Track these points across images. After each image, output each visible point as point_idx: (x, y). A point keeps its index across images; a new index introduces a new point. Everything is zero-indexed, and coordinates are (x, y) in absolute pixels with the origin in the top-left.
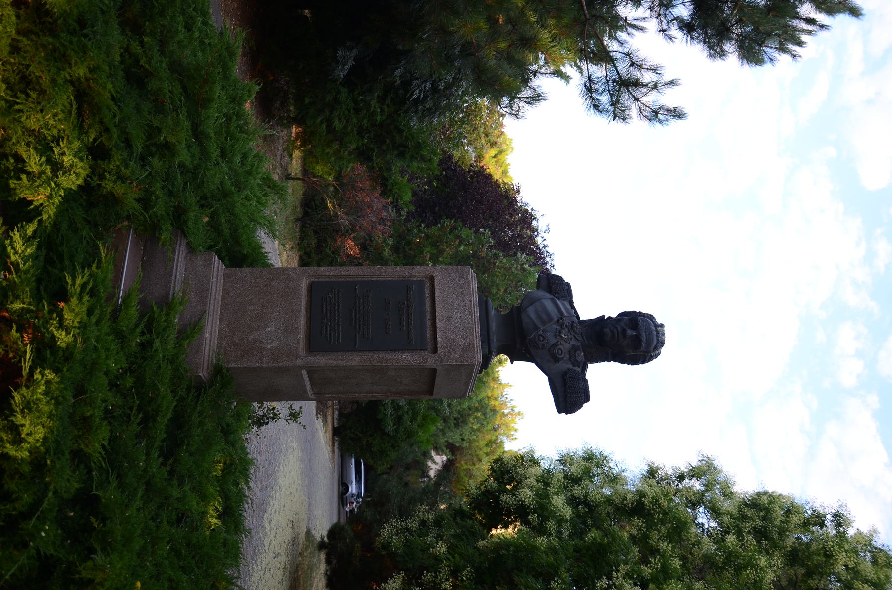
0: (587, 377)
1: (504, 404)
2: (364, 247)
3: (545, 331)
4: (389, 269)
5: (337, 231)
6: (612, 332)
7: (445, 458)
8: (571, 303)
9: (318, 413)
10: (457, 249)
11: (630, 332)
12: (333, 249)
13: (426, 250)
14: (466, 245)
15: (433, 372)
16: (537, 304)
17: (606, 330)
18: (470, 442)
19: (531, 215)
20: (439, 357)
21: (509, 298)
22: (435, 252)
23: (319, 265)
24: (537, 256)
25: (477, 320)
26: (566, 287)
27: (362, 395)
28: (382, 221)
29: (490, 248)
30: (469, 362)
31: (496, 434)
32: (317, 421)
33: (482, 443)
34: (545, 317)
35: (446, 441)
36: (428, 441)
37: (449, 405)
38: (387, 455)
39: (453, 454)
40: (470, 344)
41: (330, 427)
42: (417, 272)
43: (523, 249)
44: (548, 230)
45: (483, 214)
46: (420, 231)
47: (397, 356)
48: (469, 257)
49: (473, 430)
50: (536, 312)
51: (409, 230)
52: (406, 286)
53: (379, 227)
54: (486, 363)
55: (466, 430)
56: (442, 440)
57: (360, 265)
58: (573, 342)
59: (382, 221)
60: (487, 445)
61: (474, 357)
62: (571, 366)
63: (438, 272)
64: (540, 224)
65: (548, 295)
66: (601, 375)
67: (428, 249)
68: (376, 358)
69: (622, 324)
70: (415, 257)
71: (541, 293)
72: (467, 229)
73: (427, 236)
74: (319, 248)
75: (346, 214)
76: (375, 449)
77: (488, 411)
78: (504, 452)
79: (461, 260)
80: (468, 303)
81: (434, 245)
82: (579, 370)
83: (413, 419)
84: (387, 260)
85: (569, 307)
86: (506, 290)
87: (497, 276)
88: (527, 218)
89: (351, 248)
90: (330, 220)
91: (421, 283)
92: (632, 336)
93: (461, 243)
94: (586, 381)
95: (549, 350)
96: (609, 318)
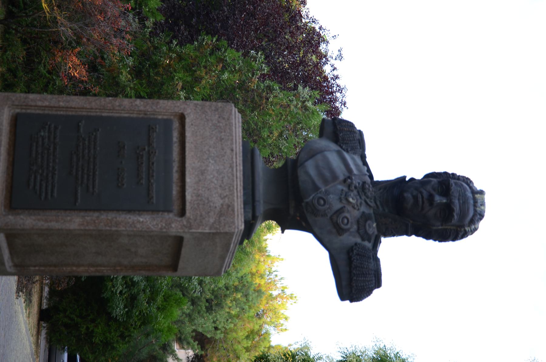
0: (379, 255)
1: (272, 284)
2: (93, 68)
4: (126, 102)
5: (56, 43)
6: (415, 198)
7: (191, 353)
8: (363, 157)
9: (19, 290)
10: (218, 77)
11: (438, 199)
12: (49, 67)
13: (178, 76)
14: (231, 72)
15: (179, 241)
16: (319, 157)
17: (408, 195)
18: (226, 332)
19: (319, 35)
20: (188, 222)
21: (284, 145)
22: (189, 79)
23: (29, 91)
24: (325, 90)
25: (240, 174)
26: (357, 136)
27: (81, 269)
28: (118, 33)
29: (263, 77)
30: (227, 229)
31: (261, 322)
32: (17, 301)
33: (242, 334)
34: (327, 174)
35: (194, 331)
36: (170, 329)
37: (200, 283)
38: (113, 348)
39: (203, 348)
40: (229, 206)
41: (35, 309)
42: (164, 108)
43: (307, 80)
44: (340, 57)
45: (256, 30)
46: (170, 50)
47: (131, 218)
48: (234, 89)
49: (231, 316)
50: (317, 167)
51: (156, 48)
52: (149, 126)
53: (114, 41)
54: (248, 232)
55: (221, 315)
56: (188, 329)
57: (85, 93)
58: (363, 209)
59: (118, 33)
60: (247, 337)
61: (233, 223)
62: (359, 240)
63: (192, 110)
64: (330, 48)
65: (333, 146)
66: (397, 253)
67: (180, 75)
68: (104, 220)
69: (429, 188)
70: (162, 84)
71: (325, 143)
72: (234, 51)
73: (180, 58)
74: (30, 63)
75: (70, 19)
76: (96, 340)
77: (251, 291)
78: (270, 347)
79: (224, 94)
80: (229, 152)
81: (189, 69)
83: (151, 300)
84: (125, 86)
85: (360, 163)
86: (281, 135)
88: (313, 39)
89: (74, 66)
90: (46, 26)
91: (167, 123)
92: (441, 204)
93: (224, 69)
94: (377, 261)
95: (331, 218)
96: (412, 179)
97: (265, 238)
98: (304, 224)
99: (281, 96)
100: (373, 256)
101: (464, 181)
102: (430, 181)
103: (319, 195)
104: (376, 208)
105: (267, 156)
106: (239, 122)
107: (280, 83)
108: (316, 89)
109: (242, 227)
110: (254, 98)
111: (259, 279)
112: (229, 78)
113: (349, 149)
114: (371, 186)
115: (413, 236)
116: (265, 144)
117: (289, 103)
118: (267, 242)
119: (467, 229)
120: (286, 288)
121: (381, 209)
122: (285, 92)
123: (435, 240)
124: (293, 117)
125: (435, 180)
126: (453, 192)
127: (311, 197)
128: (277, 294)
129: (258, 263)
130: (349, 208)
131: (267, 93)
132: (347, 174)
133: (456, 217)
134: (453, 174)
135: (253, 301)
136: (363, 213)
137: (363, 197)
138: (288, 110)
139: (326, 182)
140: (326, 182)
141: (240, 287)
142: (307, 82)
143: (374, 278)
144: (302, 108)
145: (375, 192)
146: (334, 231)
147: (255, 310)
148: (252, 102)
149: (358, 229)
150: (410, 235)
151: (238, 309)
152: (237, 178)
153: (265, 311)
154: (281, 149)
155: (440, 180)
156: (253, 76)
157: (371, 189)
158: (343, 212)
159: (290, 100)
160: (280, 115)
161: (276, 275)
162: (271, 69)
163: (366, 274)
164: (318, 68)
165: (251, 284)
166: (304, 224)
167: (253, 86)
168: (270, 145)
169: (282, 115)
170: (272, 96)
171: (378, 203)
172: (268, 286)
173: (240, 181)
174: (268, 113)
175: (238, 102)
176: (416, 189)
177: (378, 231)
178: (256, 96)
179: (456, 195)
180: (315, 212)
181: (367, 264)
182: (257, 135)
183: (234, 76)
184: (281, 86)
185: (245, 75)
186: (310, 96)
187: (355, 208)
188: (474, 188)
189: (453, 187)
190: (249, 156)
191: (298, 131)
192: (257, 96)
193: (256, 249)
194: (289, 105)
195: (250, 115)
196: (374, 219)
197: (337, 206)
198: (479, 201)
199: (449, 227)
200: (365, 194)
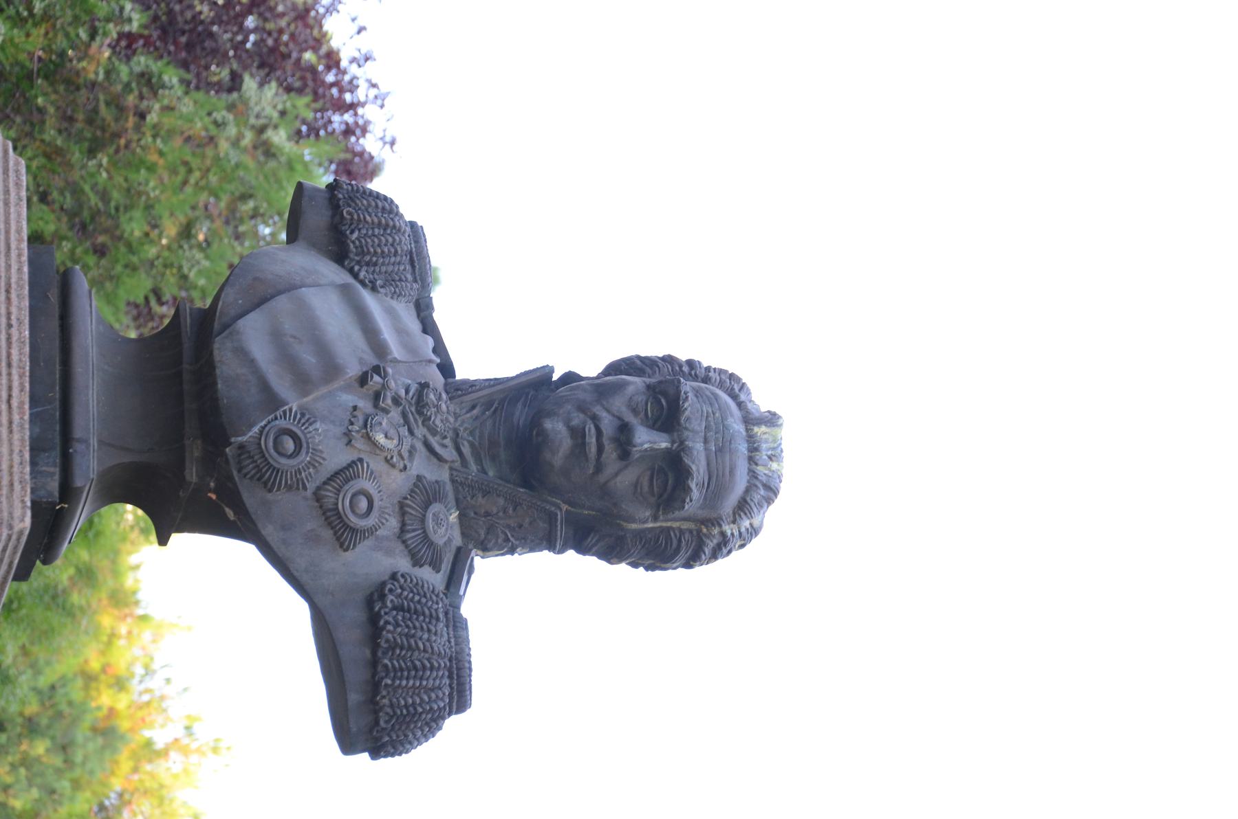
0: (466, 610)
1: (149, 707)
3: (307, 417)
6: (578, 434)
8: (423, 309)
17: (555, 427)
26: (406, 244)
29: (128, 44)
34: (308, 358)
43: (270, 61)
48: (29, 77)
58: (421, 466)
62: (403, 564)
65: (331, 272)
66: (529, 608)
69: (619, 404)
82: (434, 579)
85: (414, 326)
86: (187, 232)
87: (151, 169)
92: (653, 454)
94: (457, 625)
96: (570, 378)
97: (133, 559)
98: (230, 514)
99: (187, 106)
100: (446, 613)
101: (721, 385)
102: (621, 386)
103: (282, 423)
104: (457, 465)
105: (141, 300)
106: (18, 185)
107: (185, 65)
108: (300, 91)
109: (25, 523)
110: (95, 111)
111: (111, 692)
112: (11, 40)
113: (379, 283)
114: (444, 396)
115: (571, 553)
116: (135, 259)
117: (213, 131)
118: (140, 574)
119: (728, 529)
120: (196, 719)
121: (474, 467)
122: (200, 95)
123: (635, 565)
124: (226, 178)
125: (636, 383)
126: (688, 419)
127: (256, 429)
128: (170, 739)
129: (109, 643)
130: (376, 464)
131: (141, 97)
132: (372, 360)
133: (695, 494)
134: (690, 363)
135: (89, 766)
136: (419, 478)
137: (420, 431)
138: (210, 152)
139: (303, 382)
140: (303, 382)
141: (44, 721)
142: (272, 69)
143: (446, 681)
144: (255, 147)
145: (456, 416)
146: (327, 534)
147: (94, 793)
148: (90, 121)
149: (403, 529)
150: (561, 551)
151: (35, 793)
152: (9, 365)
153: (127, 797)
154: (184, 277)
155: (653, 380)
156: (92, 36)
157: (444, 407)
158: (357, 476)
159: (215, 123)
160: (182, 170)
161: (168, 681)
162: (156, 18)
163: (424, 667)
164: (307, 26)
165: (80, 710)
166: (230, 514)
167: (93, 70)
168: (152, 264)
169: (190, 171)
170: (157, 106)
171: (466, 450)
172: (140, 714)
173: (21, 376)
174: (142, 162)
175: (43, 122)
176: (582, 408)
177: (464, 534)
178: (102, 107)
179: (697, 425)
180: (267, 477)
181: (426, 636)
182: (106, 231)
183: (28, 35)
184: (188, 77)
185: (67, 35)
186: (283, 113)
187: (393, 467)
188: (750, 406)
189: (691, 407)
190: (54, 297)
191: (241, 221)
192: (108, 104)
193: (104, 595)
194: (211, 139)
195: (84, 167)
196: (451, 496)
197: (336, 457)
198: (764, 446)
199: (676, 525)
200: (426, 420)
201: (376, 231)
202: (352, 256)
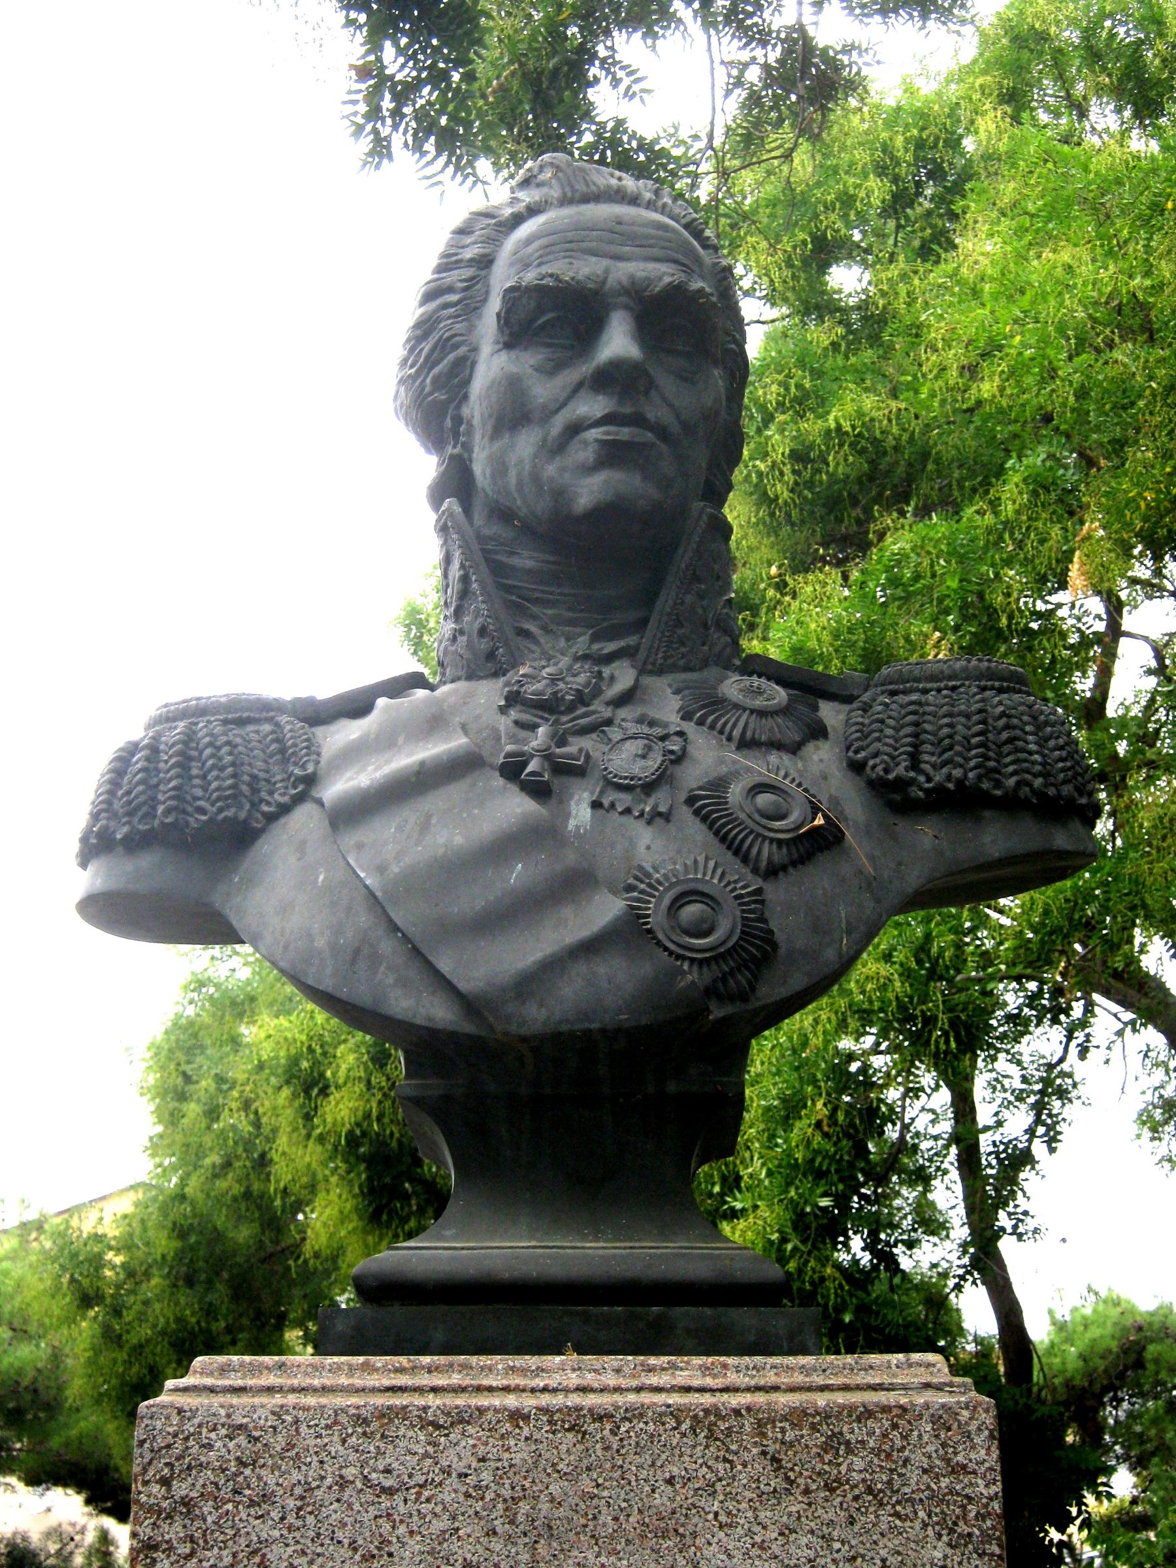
173: (651, 1370)
201: (195, 772)
202: (243, 815)
